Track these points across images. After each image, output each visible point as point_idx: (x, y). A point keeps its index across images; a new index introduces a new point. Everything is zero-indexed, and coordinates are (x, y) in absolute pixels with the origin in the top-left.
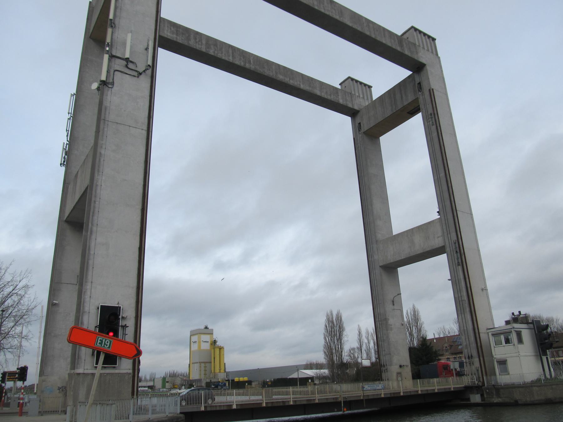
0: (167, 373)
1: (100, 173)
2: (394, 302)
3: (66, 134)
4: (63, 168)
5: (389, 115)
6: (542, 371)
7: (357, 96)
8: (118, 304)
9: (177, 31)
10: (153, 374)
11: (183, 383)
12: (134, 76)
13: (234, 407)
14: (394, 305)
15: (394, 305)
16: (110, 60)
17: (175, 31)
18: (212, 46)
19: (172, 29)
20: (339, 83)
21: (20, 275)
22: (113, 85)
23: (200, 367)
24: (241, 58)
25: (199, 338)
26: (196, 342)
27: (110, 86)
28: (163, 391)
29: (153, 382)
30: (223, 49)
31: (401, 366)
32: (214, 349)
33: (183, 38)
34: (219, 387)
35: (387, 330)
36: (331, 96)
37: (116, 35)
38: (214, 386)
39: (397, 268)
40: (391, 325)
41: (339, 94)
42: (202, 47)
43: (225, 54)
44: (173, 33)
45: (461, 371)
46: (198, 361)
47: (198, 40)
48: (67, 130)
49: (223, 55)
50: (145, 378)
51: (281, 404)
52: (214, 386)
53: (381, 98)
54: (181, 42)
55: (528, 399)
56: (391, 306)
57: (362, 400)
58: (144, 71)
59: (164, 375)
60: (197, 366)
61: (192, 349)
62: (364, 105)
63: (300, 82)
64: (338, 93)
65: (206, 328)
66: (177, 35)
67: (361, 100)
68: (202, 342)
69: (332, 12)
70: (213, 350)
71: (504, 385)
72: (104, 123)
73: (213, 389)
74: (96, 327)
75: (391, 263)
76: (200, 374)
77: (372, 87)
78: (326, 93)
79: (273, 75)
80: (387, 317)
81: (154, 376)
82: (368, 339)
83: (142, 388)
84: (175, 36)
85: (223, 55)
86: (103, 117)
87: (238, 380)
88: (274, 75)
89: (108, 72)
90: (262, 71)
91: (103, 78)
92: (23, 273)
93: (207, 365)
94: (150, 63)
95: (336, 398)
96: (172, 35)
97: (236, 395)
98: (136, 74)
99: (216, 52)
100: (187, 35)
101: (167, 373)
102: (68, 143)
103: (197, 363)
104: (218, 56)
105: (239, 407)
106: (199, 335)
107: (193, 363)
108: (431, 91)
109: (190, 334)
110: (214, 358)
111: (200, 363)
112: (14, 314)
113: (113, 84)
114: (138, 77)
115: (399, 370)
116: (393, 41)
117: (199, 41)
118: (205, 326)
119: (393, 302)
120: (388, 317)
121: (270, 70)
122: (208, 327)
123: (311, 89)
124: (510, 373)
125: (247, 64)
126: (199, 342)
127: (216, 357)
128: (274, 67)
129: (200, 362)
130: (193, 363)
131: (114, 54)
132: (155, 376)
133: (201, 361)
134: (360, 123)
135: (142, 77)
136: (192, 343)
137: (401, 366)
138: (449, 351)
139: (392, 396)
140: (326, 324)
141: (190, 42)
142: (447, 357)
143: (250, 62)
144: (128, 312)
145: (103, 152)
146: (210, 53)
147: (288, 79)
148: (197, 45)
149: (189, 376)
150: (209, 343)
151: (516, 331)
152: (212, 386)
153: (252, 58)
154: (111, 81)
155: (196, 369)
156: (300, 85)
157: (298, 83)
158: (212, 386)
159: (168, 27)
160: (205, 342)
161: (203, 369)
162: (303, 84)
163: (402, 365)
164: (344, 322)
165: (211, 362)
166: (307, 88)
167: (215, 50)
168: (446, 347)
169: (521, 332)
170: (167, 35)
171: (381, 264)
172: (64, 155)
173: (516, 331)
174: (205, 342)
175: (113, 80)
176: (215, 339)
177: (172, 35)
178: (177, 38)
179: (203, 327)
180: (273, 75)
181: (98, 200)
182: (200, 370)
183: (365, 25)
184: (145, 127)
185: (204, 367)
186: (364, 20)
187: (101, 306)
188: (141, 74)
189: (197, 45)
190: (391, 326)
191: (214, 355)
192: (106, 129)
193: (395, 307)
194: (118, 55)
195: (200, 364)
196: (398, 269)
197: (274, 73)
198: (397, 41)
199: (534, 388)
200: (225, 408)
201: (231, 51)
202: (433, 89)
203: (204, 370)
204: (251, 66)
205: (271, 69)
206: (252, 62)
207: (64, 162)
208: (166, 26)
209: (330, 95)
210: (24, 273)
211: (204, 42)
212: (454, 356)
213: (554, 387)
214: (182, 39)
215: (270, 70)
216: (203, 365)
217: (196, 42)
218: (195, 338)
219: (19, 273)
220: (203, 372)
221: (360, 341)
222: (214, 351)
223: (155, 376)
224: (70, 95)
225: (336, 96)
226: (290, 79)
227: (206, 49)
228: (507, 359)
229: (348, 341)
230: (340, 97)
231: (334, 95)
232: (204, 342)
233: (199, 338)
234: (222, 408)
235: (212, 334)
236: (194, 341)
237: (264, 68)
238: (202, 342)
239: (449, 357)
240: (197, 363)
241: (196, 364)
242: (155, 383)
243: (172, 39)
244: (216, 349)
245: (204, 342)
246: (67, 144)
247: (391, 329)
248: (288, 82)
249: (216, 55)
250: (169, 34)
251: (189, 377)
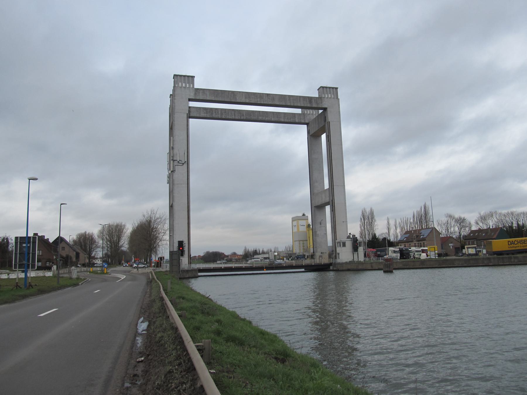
4: (168, 184)
9: (207, 111)
11: (287, 255)
14: (321, 224)
15: (321, 224)
16: (173, 162)
17: (206, 112)
18: (224, 114)
19: (205, 111)
20: (317, 89)
23: (300, 244)
26: (296, 226)
30: (229, 113)
31: (322, 253)
32: (309, 230)
34: (299, 259)
35: (316, 237)
37: (174, 152)
41: (296, 117)
49: (229, 116)
54: (209, 117)
56: (319, 225)
58: (185, 163)
60: (297, 243)
63: (272, 117)
65: (304, 215)
66: (207, 114)
67: (311, 116)
68: (300, 226)
76: (300, 249)
77: (338, 88)
82: (396, 226)
84: (206, 115)
85: (229, 116)
89: (173, 167)
92: (163, 214)
93: (305, 242)
94: (186, 160)
97: (245, 264)
98: (182, 164)
99: (226, 116)
103: (297, 241)
104: (227, 118)
107: (294, 241)
108: (329, 123)
111: (299, 241)
115: (321, 255)
116: (305, 102)
119: (321, 223)
122: (305, 214)
126: (298, 226)
129: (299, 241)
130: (294, 241)
134: (309, 130)
135: (184, 165)
136: (293, 227)
137: (322, 253)
138: (416, 239)
145: (174, 195)
156: (271, 119)
160: (302, 225)
161: (302, 245)
162: (273, 118)
163: (323, 252)
165: (307, 240)
166: (276, 119)
167: (225, 115)
169: (345, 242)
170: (202, 115)
171: (314, 206)
173: (342, 242)
174: (302, 225)
176: (309, 223)
177: (204, 115)
179: (301, 215)
180: (256, 118)
182: (300, 246)
186: (287, 97)
188: (183, 164)
189: (217, 116)
195: (299, 242)
197: (257, 117)
198: (308, 101)
203: (303, 246)
204: (244, 117)
206: (244, 115)
209: (290, 119)
211: (220, 112)
213: (351, 264)
215: (254, 116)
216: (301, 242)
217: (216, 114)
218: (295, 223)
220: (302, 248)
221: (389, 229)
226: (266, 117)
227: (221, 116)
228: (340, 253)
230: (296, 118)
234: (219, 268)
235: (308, 219)
238: (300, 226)
239: (415, 243)
240: (297, 241)
241: (296, 242)
244: (310, 231)
247: (318, 236)
249: (226, 118)
250: (203, 115)
251: (293, 251)
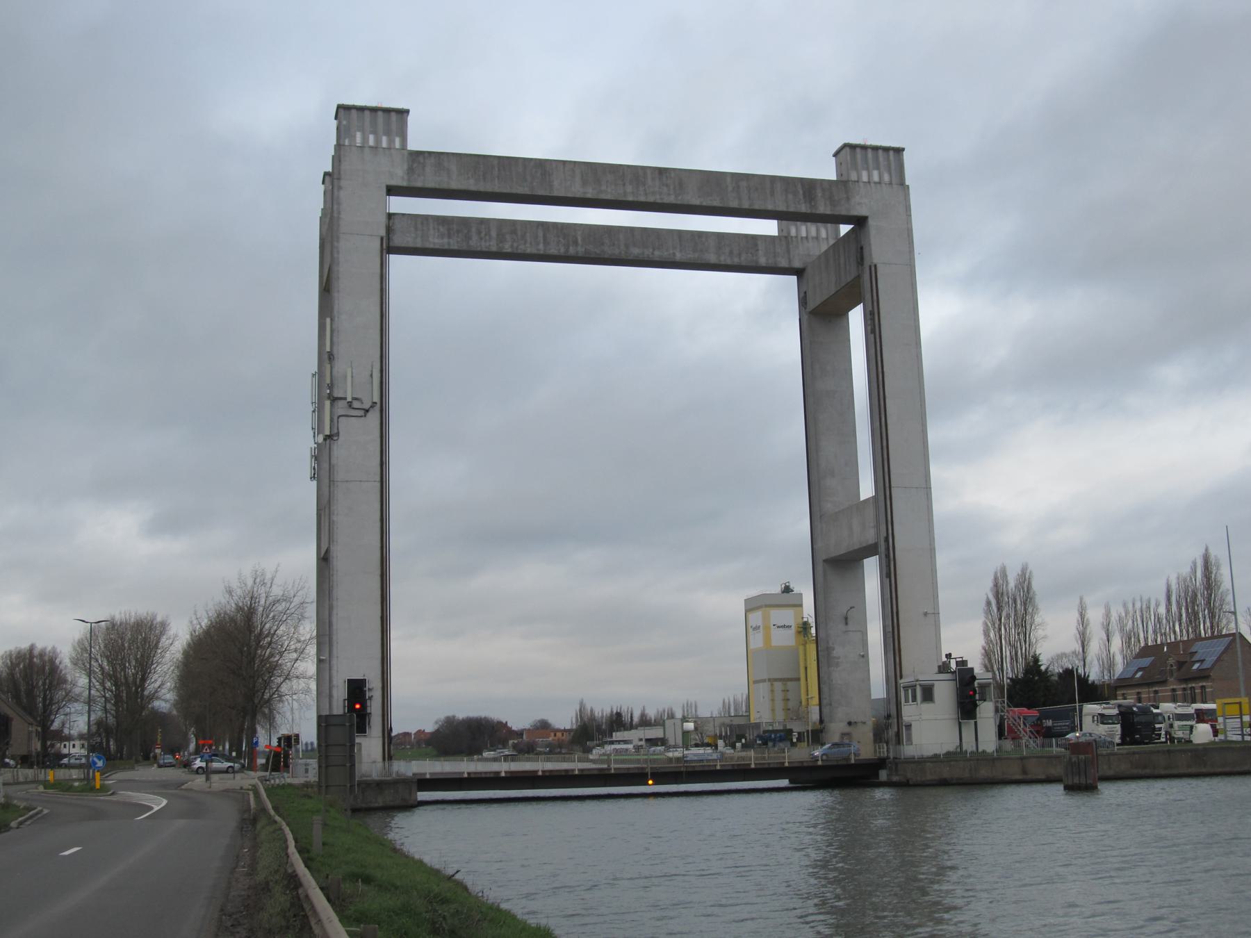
0: (727, 701)
1: (335, 543)
2: (849, 620)
3: (312, 434)
4: (315, 482)
5: (833, 293)
6: (380, 758)
7: (802, 238)
8: (364, 676)
10: (691, 707)
12: (361, 416)
13: (503, 774)
14: (847, 624)
16: (332, 405)
18: (508, 237)
21: (293, 586)
22: (338, 436)
23: (772, 691)
24: (560, 241)
25: (766, 618)
27: (335, 438)
28: (654, 751)
29: (662, 730)
30: (528, 234)
31: (850, 723)
32: (805, 644)
33: (459, 240)
34: (770, 744)
36: (740, 258)
37: (335, 370)
38: (760, 742)
39: (863, 559)
40: (839, 658)
41: (760, 248)
42: (491, 243)
43: (531, 244)
44: (442, 236)
45: (1054, 726)
46: (765, 677)
47: (483, 235)
48: (313, 428)
49: (528, 245)
50: (643, 715)
51: (563, 774)
52: (760, 742)
53: (844, 236)
55: (919, 779)
57: (682, 772)
59: (721, 706)
60: (763, 689)
61: (752, 646)
62: (817, 253)
64: (756, 245)
65: (787, 590)
66: (449, 237)
69: (661, 194)
70: (801, 648)
71: (905, 759)
72: (334, 484)
73: (1182, 738)
74: (345, 700)
75: (840, 556)
76: (773, 710)
78: (731, 253)
79: (620, 253)
80: (831, 645)
81: (694, 711)
83: (619, 744)
84: (446, 240)
86: (332, 479)
87: (314, 763)
88: (623, 252)
89: (332, 420)
90: (598, 252)
91: (327, 432)
94: (376, 399)
95: (642, 768)
96: (441, 241)
98: (362, 413)
99: (515, 245)
100: (466, 231)
101: (727, 701)
102: (316, 445)
103: (764, 681)
105: (508, 775)
106: (764, 609)
107: (756, 682)
108: (873, 269)
109: (745, 607)
110: (806, 668)
111: (772, 681)
112: (293, 647)
113: (338, 434)
114: (365, 416)
115: (847, 729)
116: (790, 196)
117: (486, 235)
118: (783, 586)
119: (846, 619)
120: (833, 644)
121: (614, 245)
122: (791, 587)
123: (696, 255)
124: (914, 743)
125: (571, 248)
127: (808, 666)
128: (621, 237)
131: (336, 395)
132: (696, 711)
133: (772, 677)
134: (805, 293)
135: (369, 414)
136: (750, 630)
137: (850, 723)
139: (736, 768)
140: (988, 598)
141: (471, 243)
142: (1172, 687)
143: (576, 243)
144: (374, 683)
146: (505, 251)
147: (651, 250)
148: (483, 243)
149: (747, 714)
150: (793, 631)
151: (920, 685)
152: (758, 742)
153: (579, 233)
154: (336, 431)
155: (764, 697)
157: (671, 252)
158: (758, 742)
159: (434, 228)
160: (782, 627)
161: (779, 696)
162: (681, 251)
163: (852, 721)
164: (1037, 593)
165: (798, 679)
166: (689, 256)
168: (1172, 666)
169: (933, 685)
170: (434, 243)
172: (313, 465)
173: (920, 685)
175: (338, 429)
176: (805, 620)
178: (449, 244)
179: (777, 589)
180: (620, 253)
181: (335, 572)
182: (773, 700)
183: (730, 188)
184: (378, 478)
185: (783, 691)
186: (729, 179)
187: (348, 680)
188: (367, 411)
190: (836, 660)
191: (806, 660)
192: (336, 492)
193: (850, 627)
194: (340, 396)
195: (772, 685)
196: (865, 560)
198: (801, 192)
199: (928, 764)
200: (492, 775)
201: (541, 234)
202: (875, 266)
205: (616, 243)
207: (314, 474)
208: (431, 228)
210: (297, 583)
211: (494, 233)
212: (1182, 686)
213: (952, 763)
214: (458, 242)
215: (614, 245)
217: (481, 239)
218: (756, 618)
219: (291, 584)
220: (779, 705)
221: (1084, 642)
222: (805, 650)
223: (696, 711)
224: (311, 376)
225: (751, 253)
226: (654, 250)
229: (1045, 637)
231: (747, 253)
232: (778, 627)
233: (766, 618)
234: (488, 776)
235: (801, 606)
236: (754, 626)
237: (603, 244)
239: (1175, 687)
240: (764, 681)
241: (761, 684)
242: (666, 730)
243: (441, 247)
244: (808, 646)
245: (778, 627)
246: (315, 448)
248: (651, 256)
250: (436, 241)
251: (749, 716)
